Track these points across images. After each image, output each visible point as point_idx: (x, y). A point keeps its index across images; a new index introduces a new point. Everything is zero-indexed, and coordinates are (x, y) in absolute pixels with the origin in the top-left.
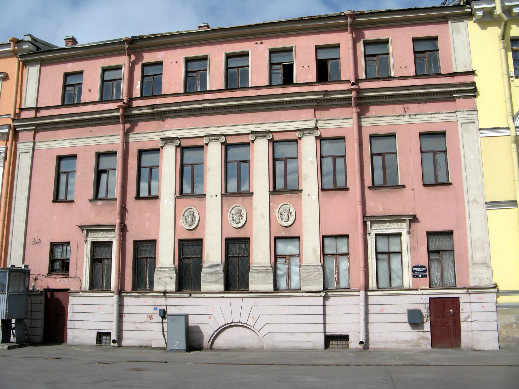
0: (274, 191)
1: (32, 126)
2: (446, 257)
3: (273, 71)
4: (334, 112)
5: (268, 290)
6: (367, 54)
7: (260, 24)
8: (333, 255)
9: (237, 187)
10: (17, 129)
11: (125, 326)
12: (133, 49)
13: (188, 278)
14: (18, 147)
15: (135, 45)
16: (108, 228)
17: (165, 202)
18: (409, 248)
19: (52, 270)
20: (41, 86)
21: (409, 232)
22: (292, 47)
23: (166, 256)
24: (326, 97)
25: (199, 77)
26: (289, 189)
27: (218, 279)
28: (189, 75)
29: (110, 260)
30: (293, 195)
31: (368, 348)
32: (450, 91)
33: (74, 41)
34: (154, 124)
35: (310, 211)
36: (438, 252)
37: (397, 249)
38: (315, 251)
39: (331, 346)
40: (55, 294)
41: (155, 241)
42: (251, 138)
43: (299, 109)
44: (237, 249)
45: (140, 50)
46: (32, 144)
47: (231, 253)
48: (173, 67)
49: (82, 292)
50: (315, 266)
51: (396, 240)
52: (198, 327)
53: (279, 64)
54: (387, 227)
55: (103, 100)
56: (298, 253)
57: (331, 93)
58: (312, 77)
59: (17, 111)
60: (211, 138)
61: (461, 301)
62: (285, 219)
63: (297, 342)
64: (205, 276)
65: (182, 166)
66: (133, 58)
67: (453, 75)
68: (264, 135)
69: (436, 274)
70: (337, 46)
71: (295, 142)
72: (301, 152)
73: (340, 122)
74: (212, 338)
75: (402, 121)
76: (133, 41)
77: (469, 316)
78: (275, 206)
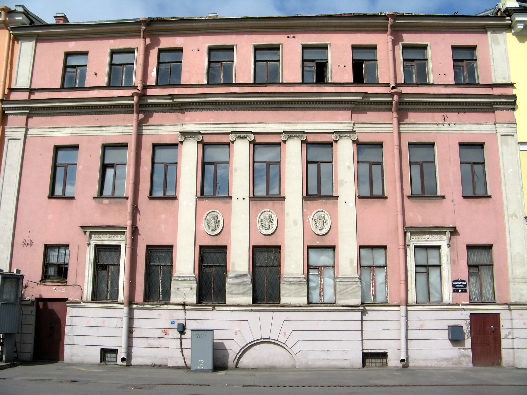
0: (308, 197)
1: (26, 110)
2: (484, 272)
3: (305, 68)
4: (371, 116)
5: (301, 304)
6: (305, 58)
7: (295, 17)
8: (370, 267)
9: (267, 189)
10: (6, 112)
11: (136, 342)
12: (148, 31)
13: (211, 288)
14: (6, 133)
15: (152, 28)
16: (119, 230)
17: (185, 203)
18: (449, 262)
19: (45, 277)
20: (35, 66)
21: (449, 245)
22: (327, 45)
23: (185, 264)
24: (365, 100)
25: (222, 68)
26: (322, 194)
27: (245, 290)
28: (212, 65)
29: (117, 267)
30: (328, 201)
31: (408, 367)
32: (491, 103)
33: (65, 18)
34: (172, 116)
35: (348, 221)
36: (477, 266)
37: (435, 262)
38: (351, 262)
39: (367, 364)
40: (49, 304)
41: (172, 247)
42: (283, 137)
43: (335, 110)
44: (266, 258)
45: (399, 29)
46: (24, 130)
47: (259, 262)
48: (194, 56)
49: (84, 302)
50: (352, 278)
51: (434, 253)
52: (222, 344)
53: (313, 61)
54: (426, 239)
55: (111, 85)
56: (332, 264)
57: (405, 96)
58: (349, 77)
59: (6, 92)
60: (238, 135)
61: (501, 317)
62: (320, 227)
63: (333, 360)
64: (230, 287)
65: (204, 164)
66: (148, 41)
67: (492, 86)
68: (297, 135)
69: (473, 287)
70: (374, 48)
71: (227, 146)
72: (337, 156)
73: (377, 126)
74: (238, 356)
75: (441, 129)
76: (150, 22)
77: (509, 333)
78: (309, 213)
